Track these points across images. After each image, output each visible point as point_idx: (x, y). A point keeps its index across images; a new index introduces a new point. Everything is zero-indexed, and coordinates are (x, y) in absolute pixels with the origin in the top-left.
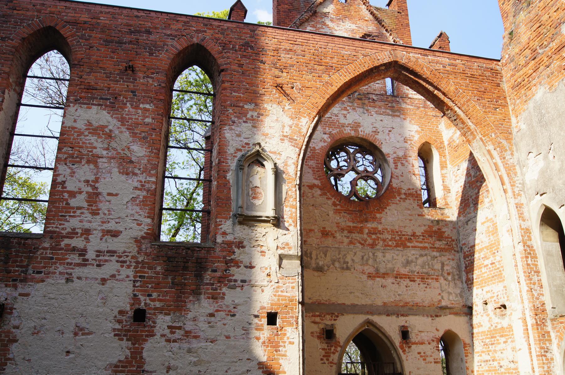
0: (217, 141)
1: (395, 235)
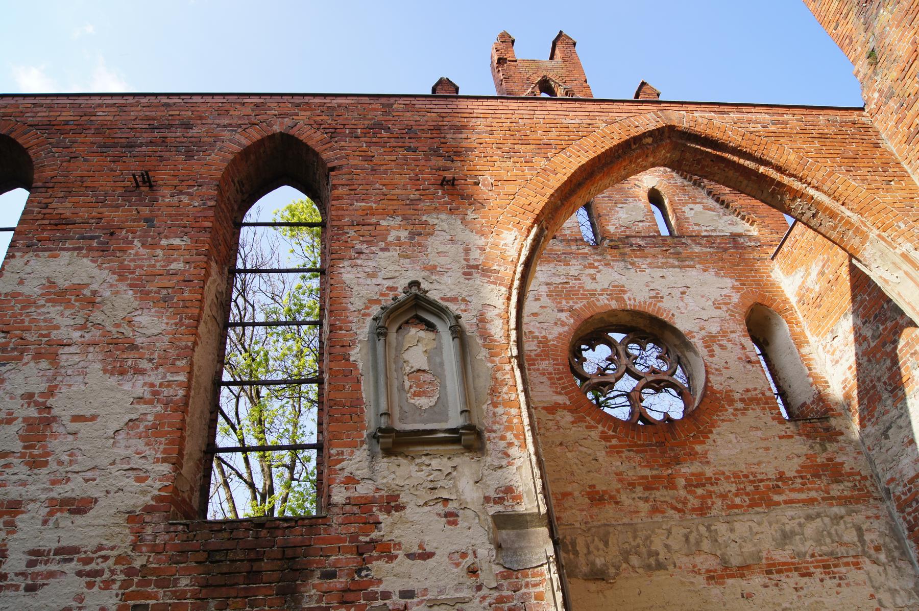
1: (743, 483)
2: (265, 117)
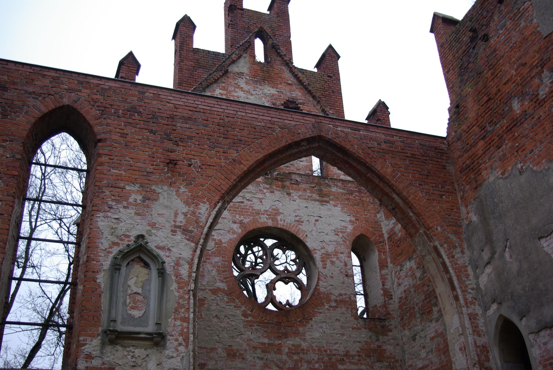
0: (86, 231)
2: (59, 89)
